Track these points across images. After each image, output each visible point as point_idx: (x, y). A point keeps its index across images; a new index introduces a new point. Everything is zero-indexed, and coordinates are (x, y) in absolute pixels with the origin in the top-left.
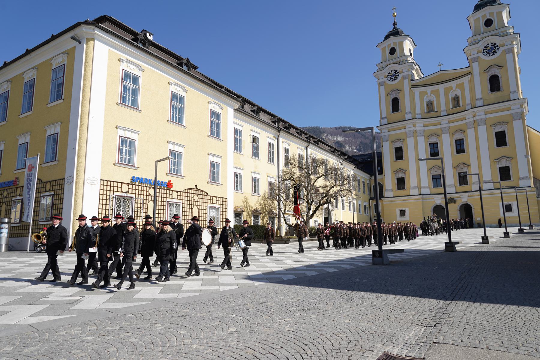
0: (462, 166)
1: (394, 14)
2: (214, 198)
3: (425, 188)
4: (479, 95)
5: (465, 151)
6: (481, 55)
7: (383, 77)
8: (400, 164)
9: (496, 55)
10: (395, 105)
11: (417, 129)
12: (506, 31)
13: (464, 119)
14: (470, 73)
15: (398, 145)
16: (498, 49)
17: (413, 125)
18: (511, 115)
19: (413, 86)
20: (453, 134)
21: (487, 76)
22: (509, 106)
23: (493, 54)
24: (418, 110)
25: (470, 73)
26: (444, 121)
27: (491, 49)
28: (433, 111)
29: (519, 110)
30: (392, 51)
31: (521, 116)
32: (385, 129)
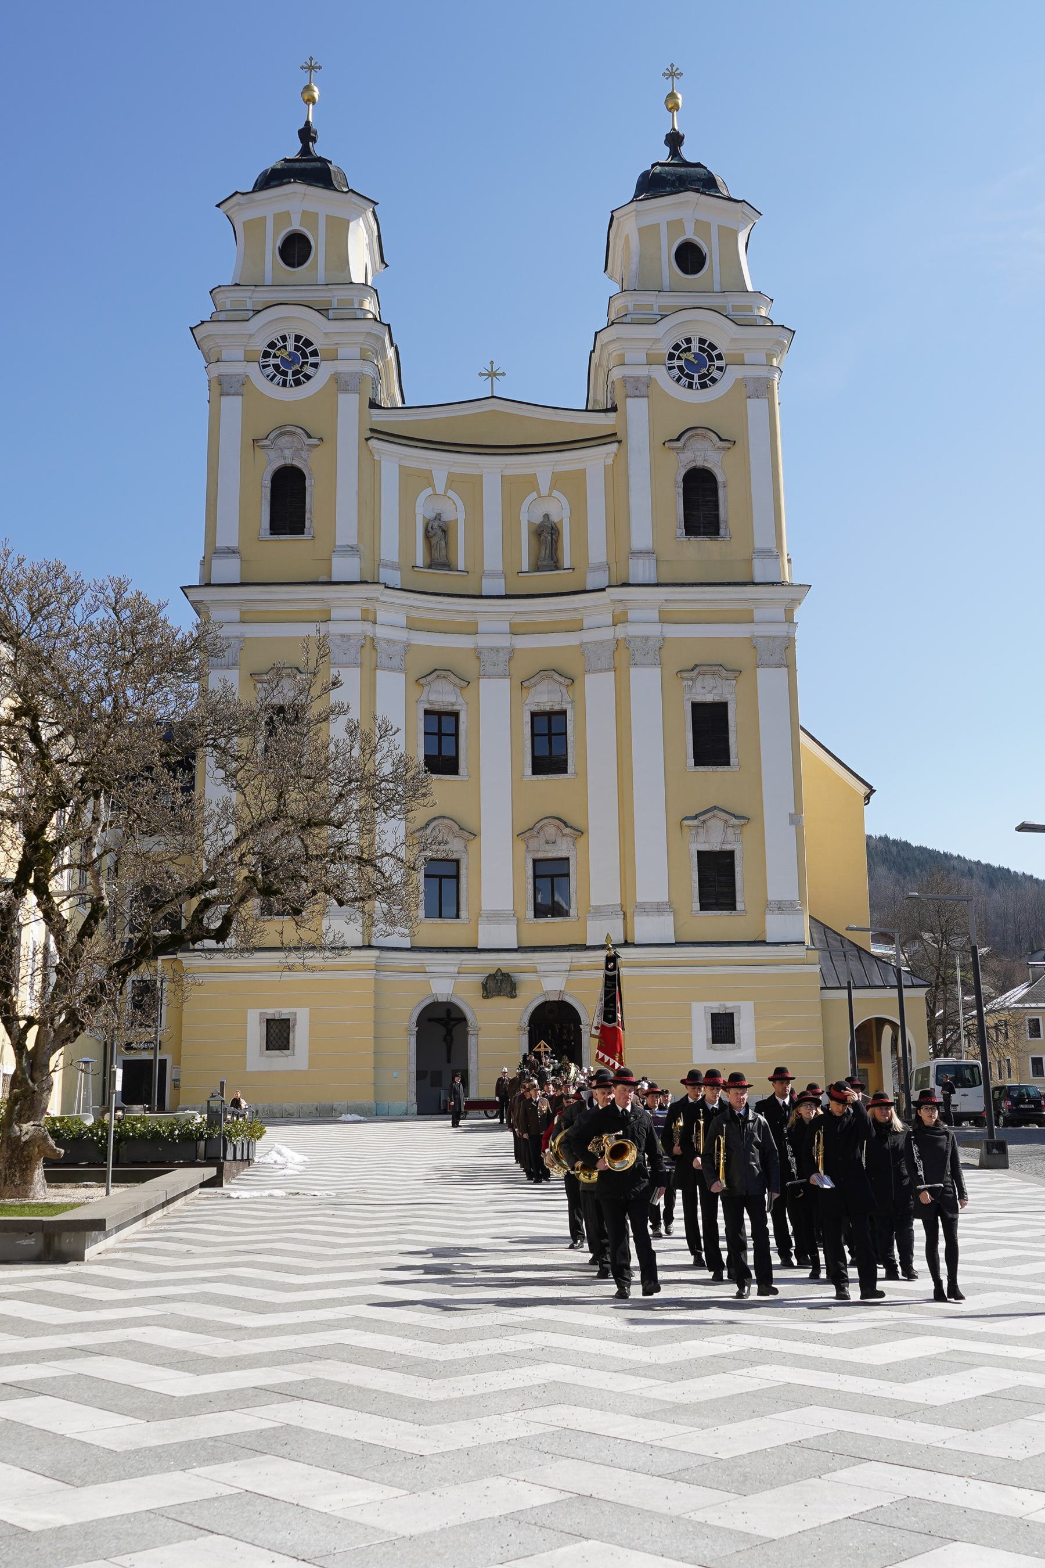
0: (551, 831)
1: (308, 88)
3: (496, 917)
4: (641, 537)
5: (570, 768)
6: (662, 377)
7: (356, 352)
9: (308, 389)
10: (288, 501)
11: (381, 632)
12: (750, 308)
13: (579, 628)
14: (610, 438)
16: (315, 365)
17: (365, 611)
18: (752, 643)
19: (377, 433)
20: (524, 685)
22: (574, 616)
24: (390, 549)
25: (610, 438)
26: (494, 619)
27: (293, 360)
28: (446, 565)
29: (779, 630)
30: (295, 249)
31: (784, 654)
32: (226, 608)
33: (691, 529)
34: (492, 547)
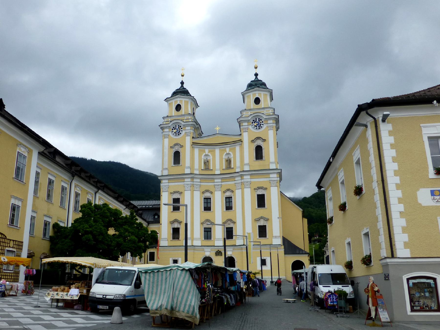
2: (12, 242)
3: (197, 239)
4: (246, 161)
15: (176, 196)
21: (254, 146)
24: (196, 166)
34: (218, 166)
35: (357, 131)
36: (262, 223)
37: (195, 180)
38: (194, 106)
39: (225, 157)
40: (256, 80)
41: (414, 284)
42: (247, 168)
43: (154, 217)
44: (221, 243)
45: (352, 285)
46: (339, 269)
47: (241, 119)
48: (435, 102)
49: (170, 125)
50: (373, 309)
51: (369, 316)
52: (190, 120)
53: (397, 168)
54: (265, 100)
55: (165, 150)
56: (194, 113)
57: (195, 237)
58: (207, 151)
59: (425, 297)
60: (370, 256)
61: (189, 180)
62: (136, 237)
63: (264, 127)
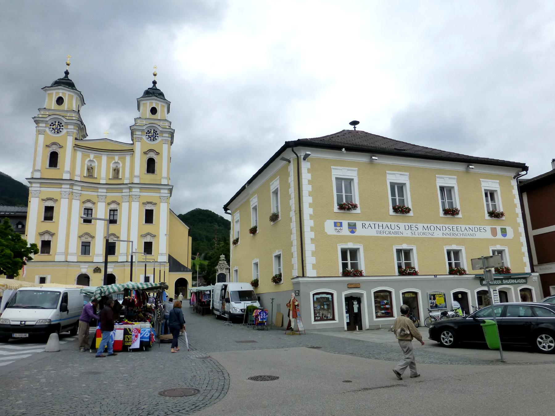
3: (72, 254)
4: (137, 172)
8: (48, 226)
15: (49, 204)
21: (146, 158)
23: (58, 132)
33: (148, 171)
35: (279, 164)
36: (148, 239)
37: (75, 187)
38: (79, 103)
39: (112, 166)
40: (154, 88)
41: (317, 298)
42: (136, 181)
43: (17, 226)
44: (102, 259)
45: (259, 301)
46: (248, 287)
47: (135, 127)
48: (344, 149)
49: (47, 119)
50: (292, 320)
51: (289, 328)
52: (74, 118)
53: (311, 202)
54: (162, 111)
55: (38, 149)
56: (79, 111)
57: (70, 251)
58: (92, 157)
59: (324, 309)
60: (280, 275)
61: (68, 186)
62: (11, 250)
63: (159, 139)
